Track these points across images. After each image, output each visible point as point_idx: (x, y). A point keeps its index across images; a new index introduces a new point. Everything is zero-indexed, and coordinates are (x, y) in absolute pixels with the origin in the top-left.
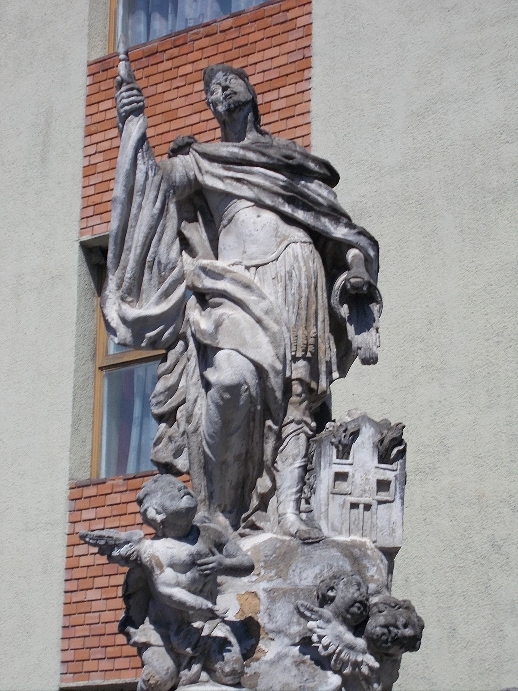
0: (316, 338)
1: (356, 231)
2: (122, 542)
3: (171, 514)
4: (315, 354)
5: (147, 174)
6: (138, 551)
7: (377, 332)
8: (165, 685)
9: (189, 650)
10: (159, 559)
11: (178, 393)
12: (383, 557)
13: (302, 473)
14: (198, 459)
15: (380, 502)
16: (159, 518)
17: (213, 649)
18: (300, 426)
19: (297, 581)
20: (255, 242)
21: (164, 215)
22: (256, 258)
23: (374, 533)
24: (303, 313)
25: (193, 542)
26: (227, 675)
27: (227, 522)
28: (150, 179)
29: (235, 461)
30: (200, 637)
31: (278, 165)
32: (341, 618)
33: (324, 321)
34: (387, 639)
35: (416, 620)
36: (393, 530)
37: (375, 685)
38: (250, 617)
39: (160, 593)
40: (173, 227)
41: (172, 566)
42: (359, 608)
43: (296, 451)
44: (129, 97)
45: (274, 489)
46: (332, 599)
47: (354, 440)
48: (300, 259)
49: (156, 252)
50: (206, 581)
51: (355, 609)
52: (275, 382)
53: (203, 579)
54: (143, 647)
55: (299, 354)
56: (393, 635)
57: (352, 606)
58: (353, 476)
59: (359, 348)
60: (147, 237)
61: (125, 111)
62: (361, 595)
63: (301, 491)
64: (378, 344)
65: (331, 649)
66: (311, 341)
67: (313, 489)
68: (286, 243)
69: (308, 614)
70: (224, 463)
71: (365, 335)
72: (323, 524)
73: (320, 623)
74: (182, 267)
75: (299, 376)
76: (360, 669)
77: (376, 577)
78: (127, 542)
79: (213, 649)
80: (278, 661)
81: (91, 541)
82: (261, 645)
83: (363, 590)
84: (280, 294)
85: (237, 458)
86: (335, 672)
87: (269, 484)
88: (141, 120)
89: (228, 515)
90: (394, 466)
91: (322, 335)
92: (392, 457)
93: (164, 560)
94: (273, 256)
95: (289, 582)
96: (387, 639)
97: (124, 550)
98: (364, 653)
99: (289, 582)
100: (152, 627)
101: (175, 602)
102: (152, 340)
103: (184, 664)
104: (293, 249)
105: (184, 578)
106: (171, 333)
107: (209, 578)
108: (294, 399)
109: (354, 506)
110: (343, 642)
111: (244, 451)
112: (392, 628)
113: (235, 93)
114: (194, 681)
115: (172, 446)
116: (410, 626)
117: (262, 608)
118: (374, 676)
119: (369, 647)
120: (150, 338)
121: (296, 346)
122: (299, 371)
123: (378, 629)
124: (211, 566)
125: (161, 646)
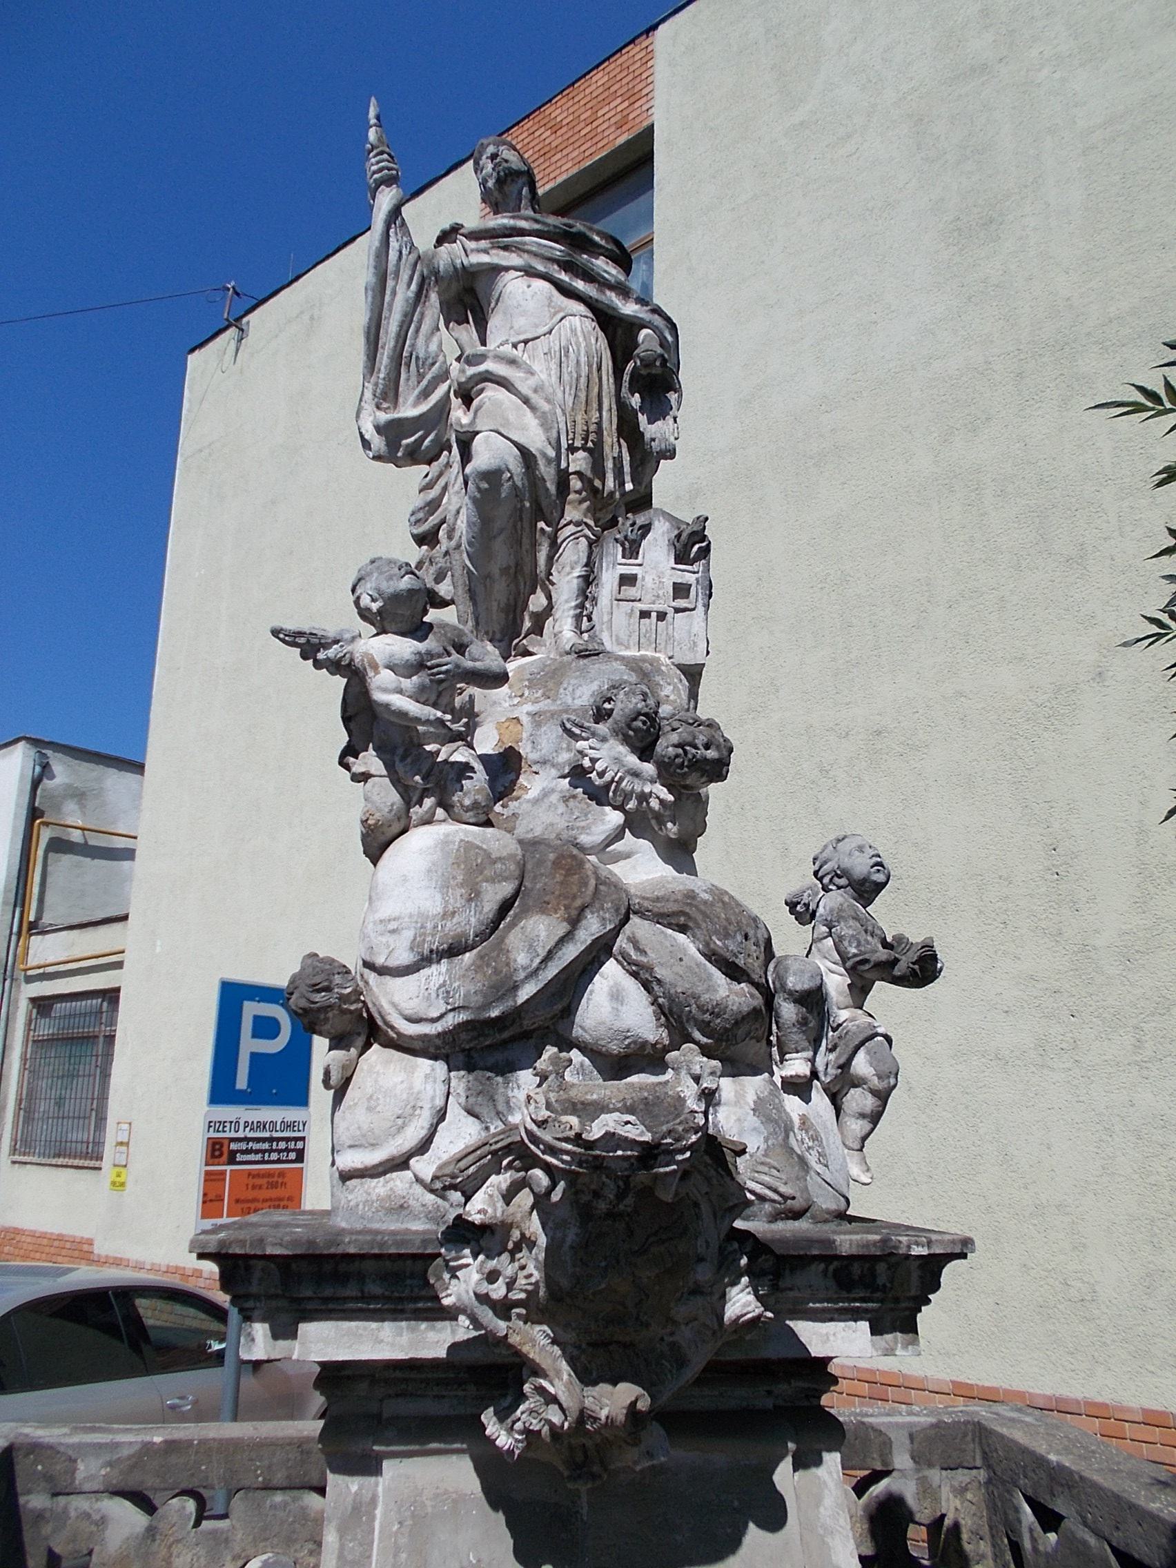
0: (599, 424)
1: (649, 308)
2: (330, 641)
3: (389, 598)
4: (599, 443)
5: (401, 252)
6: (352, 653)
7: (675, 421)
8: (390, 826)
9: (417, 778)
10: (373, 658)
11: (440, 509)
12: (683, 677)
13: (583, 585)
14: (462, 580)
15: (677, 610)
16: (375, 607)
17: (450, 777)
18: (579, 528)
19: (570, 701)
20: (524, 313)
21: (422, 301)
22: (525, 332)
23: (670, 647)
24: (583, 395)
25: (421, 639)
26: (468, 810)
27: (497, 652)
28: (404, 257)
29: (501, 575)
30: (435, 763)
31: (555, 233)
32: (621, 736)
33: (610, 410)
34: (683, 762)
35: (722, 740)
36: (694, 643)
37: (669, 825)
38: (511, 747)
39: (375, 701)
40: (433, 316)
41: (388, 667)
42: (644, 723)
43: (575, 558)
44: (378, 163)
45: (549, 610)
46: (610, 713)
47: (644, 536)
48: (579, 334)
49: (413, 346)
50: (440, 689)
51: (638, 724)
52: (547, 472)
53: (435, 686)
54: (363, 777)
55: (578, 443)
56: (690, 756)
57: (635, 719)
58: (643, 578)
59: (654, 440)
60: (401, 326)
61: (375, 180)
62: (647, 706)
63: (581, 606)
64: (676, 435)
65: (608, 777)
66: (593, 428)
67: (594, 599)
68: (562, 314)
69: (577, 731)
70: (488, 576)
71: (659, 423)
72: (605, 637)
73: (593, 742)
74: (445, 362)
75: (578, 469)
76: (648, 803)
77: (672, 697)
78: (336, 642)
79: (450, 777)
80: (543, 799)
81: (287, 638)
82: (522, 780)
83: (651, 702)
84: (553, 372)
85: (505, 571)
86: (615, 808)
87: (545, 602)
88: (395, 191)
89: (497, 644)
90: (695, 567)
91: (608, 427)
92: (692, 556)
93: (379, 659)
94: (546, 329)
95: (559, 702)
96: (683, 762)
97: (332, 652)
98: (653, 782)
99: (559, 702)
100: (374, 753)
101: (394, 712)
102: (409, 449)
103: (415, 799)
104: (570, 321)
105: (408, 684)
106: (432, 441)
107: (444, 685)
108: (572, 497)
109: (645, 614)
110: (624, 766)
111: (512, 564)
112: (688, 748)
113: (506, 161)
114: (428, 821)
115: (432, 570)
116: (713, 747)
117: (525, 735)
118: (667, 813)
119: (659, 776)
120: (408, 445)
121: (574, 433)
122: (579, 463)
123: (670, 749)
124: (444, 668)
125: (384, 776)
